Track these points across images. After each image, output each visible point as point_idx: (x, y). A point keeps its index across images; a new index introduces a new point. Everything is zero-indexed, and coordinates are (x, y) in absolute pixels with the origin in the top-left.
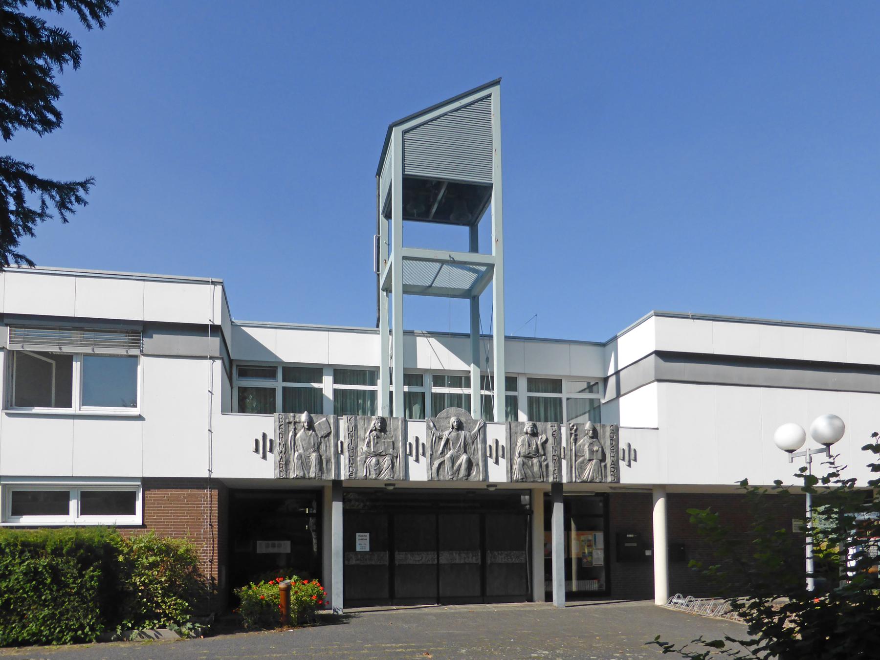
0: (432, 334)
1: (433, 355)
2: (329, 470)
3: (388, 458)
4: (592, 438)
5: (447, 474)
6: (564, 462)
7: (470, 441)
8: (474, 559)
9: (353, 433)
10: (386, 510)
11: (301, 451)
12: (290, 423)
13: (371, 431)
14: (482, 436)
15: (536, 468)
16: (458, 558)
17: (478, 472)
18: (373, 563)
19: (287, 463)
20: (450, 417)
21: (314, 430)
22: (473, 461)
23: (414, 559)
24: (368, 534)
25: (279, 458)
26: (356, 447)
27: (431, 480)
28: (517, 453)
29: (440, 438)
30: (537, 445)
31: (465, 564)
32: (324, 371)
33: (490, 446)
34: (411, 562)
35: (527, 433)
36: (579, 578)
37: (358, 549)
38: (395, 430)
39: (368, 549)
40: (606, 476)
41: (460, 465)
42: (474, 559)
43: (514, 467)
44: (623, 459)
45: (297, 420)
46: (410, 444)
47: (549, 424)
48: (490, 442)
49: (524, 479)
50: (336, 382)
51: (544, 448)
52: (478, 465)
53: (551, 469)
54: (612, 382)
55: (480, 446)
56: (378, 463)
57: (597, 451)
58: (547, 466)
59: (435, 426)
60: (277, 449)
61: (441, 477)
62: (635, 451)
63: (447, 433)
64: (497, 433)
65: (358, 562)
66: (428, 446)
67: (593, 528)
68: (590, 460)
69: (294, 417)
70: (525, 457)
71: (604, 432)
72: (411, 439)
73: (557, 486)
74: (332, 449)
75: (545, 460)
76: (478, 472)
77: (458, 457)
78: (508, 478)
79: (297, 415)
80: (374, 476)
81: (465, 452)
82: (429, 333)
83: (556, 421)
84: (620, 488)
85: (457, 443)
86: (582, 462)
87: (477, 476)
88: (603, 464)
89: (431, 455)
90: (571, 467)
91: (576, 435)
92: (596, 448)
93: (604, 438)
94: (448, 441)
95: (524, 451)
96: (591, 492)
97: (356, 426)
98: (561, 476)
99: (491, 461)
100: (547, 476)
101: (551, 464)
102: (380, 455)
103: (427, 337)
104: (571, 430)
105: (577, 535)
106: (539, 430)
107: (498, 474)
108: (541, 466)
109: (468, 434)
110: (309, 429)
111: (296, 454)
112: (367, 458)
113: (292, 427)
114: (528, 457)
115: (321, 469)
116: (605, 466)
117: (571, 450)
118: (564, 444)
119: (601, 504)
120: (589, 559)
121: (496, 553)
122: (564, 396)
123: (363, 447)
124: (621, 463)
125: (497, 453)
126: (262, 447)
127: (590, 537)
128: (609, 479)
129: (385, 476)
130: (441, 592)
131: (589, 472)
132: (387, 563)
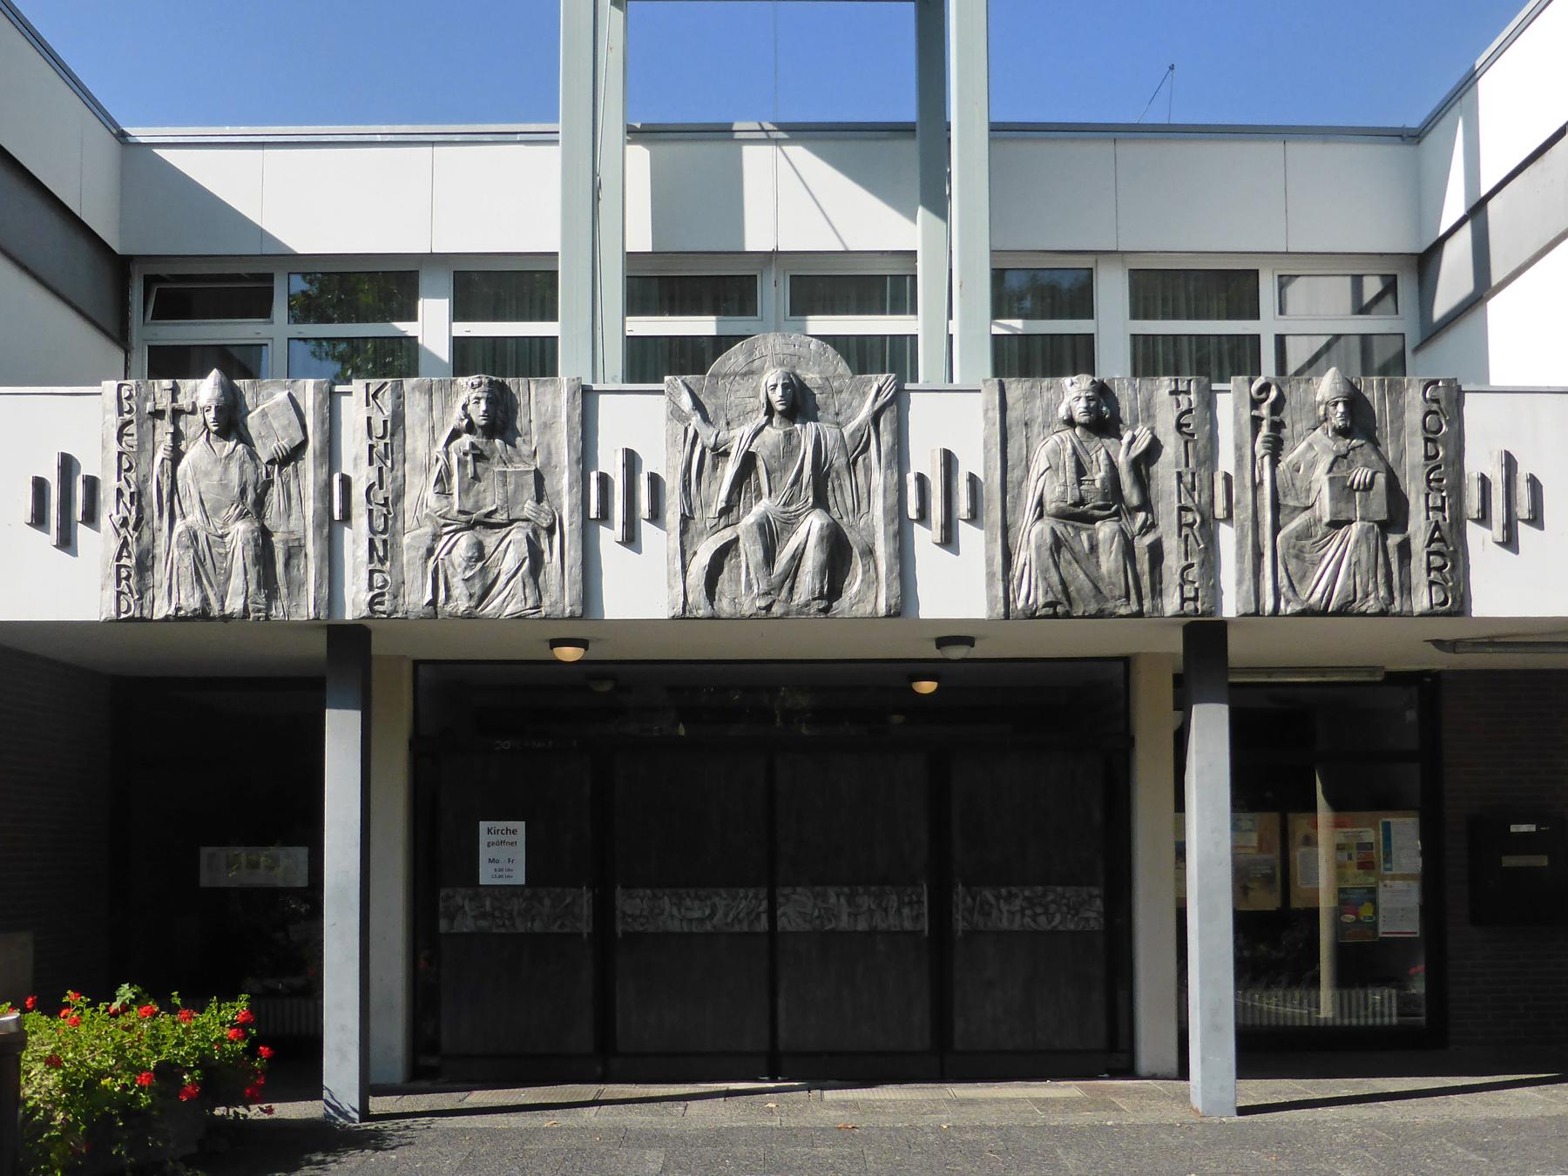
0: (798, 132)
1: (796, 203)
2: (296, 587)
3: (518, 535)
4: (1342, 432)
5: (743, 592)
6: (1227, 537)
7: (840, 462)
8: (905, 914)
9: (389, 439)
10: (516, 727)
11: (195, 517)
12: (158, 414)
13: (455, 434)
14: (886, 438)
15: (1109, 561)
16: (845, 911)
17: (870, 582)
18: (538, 927)
19: (144, 565)
20: (759, 372)
21: (245, 439)
22: (852, 537)
23: (679, 913)
24: (520, 826)
25: (115, 545)
26: (399, 495)
27: (683, 617)
28: (1030, 502)
29: (721, 453)
30: (1113, 467)
31: (872, 933)
32: (424, 282)
33: (921, 479)
34: (675, 926)
35: (1070, 422)
36: (1343, 980)
37: (486, 876)
38: (546, 427)
39: (519, 878)
40: (1407, 589)
41: (798, 557)
42: (905, 914)
43: (1019, 560)
44: (1484, 519)
45: (184, 402)
46: (604, 480)
47: (1165, 384)
48: (924, 460)
49: (1060, 607)
50: (460, 313)
51: (1142, 480)
52: (869, 552)
53: (1173, 561)
54: (1458, 253)
55: (878, 479)
56: (479, 553)
57: (1368, 487)
58: (1156, 552)
59: (698, 405)
60: (109, 511)
61: (724, 606)
62: (1534, 483)
63: (747, 430)
64: (951, 422)
65: (483, 923)
66: (673, 485)
67: (1386, 802)
68: (1336, 525)
69: (175, 391)
70: (1062, 515)
71: (1398, 413)
72: (610, 462)
73: (1206, 635)
74: (310, 507)
75: (1148, 527)
76: (870, 582)
77: (790, 523)
78: (991, 602)
79: (187, 385)
80: (461, 604)
81: (821, 502)
82: (783, 127)
83: (1199, 373)
84: (1478, 645)
85: (784, 469)
86: (1305, 533)
87: (867, 593)
88: (1394, 540)
89: (686, 520)
90: (1258, 555)
91: (1277, 427)
92: (1360, 475)
93: (1398, 433)
94: (749, 461)
95: (1057, 490)
96: (1371, 670)
97: (398, 418)
98: (1215, 591)
99: (925, 539)
100: (1157, 591)
101: (1172, 545)
102: (487, 523)
103: (777, 142)
104: (1255, 404)
105: (1338, 824)
106: (1125, 413)
107: (956, 587)
108: (1128, 551)
109: (830, 435)
110: (224, 434)
111: (180, 526)
112: (436, 537)
113: (164, 427)
114: (1077, 514)
115: (267, 582)
116: (1405, 549)
117: (1256, 487)
118: (1226, 462)
119: (1411, 715)
120: (1366, 911)
121: (988, 894)
122: (1265, 327)
123: (421, 495)
124: (1475, 535)
125: (954, 503)
126: (61, 505)
127: (1370, 835)
128: (1422, 600)
129: (508, 601)
130: (783, 1033)
131: (1336, 568)
132: (586, 928)
